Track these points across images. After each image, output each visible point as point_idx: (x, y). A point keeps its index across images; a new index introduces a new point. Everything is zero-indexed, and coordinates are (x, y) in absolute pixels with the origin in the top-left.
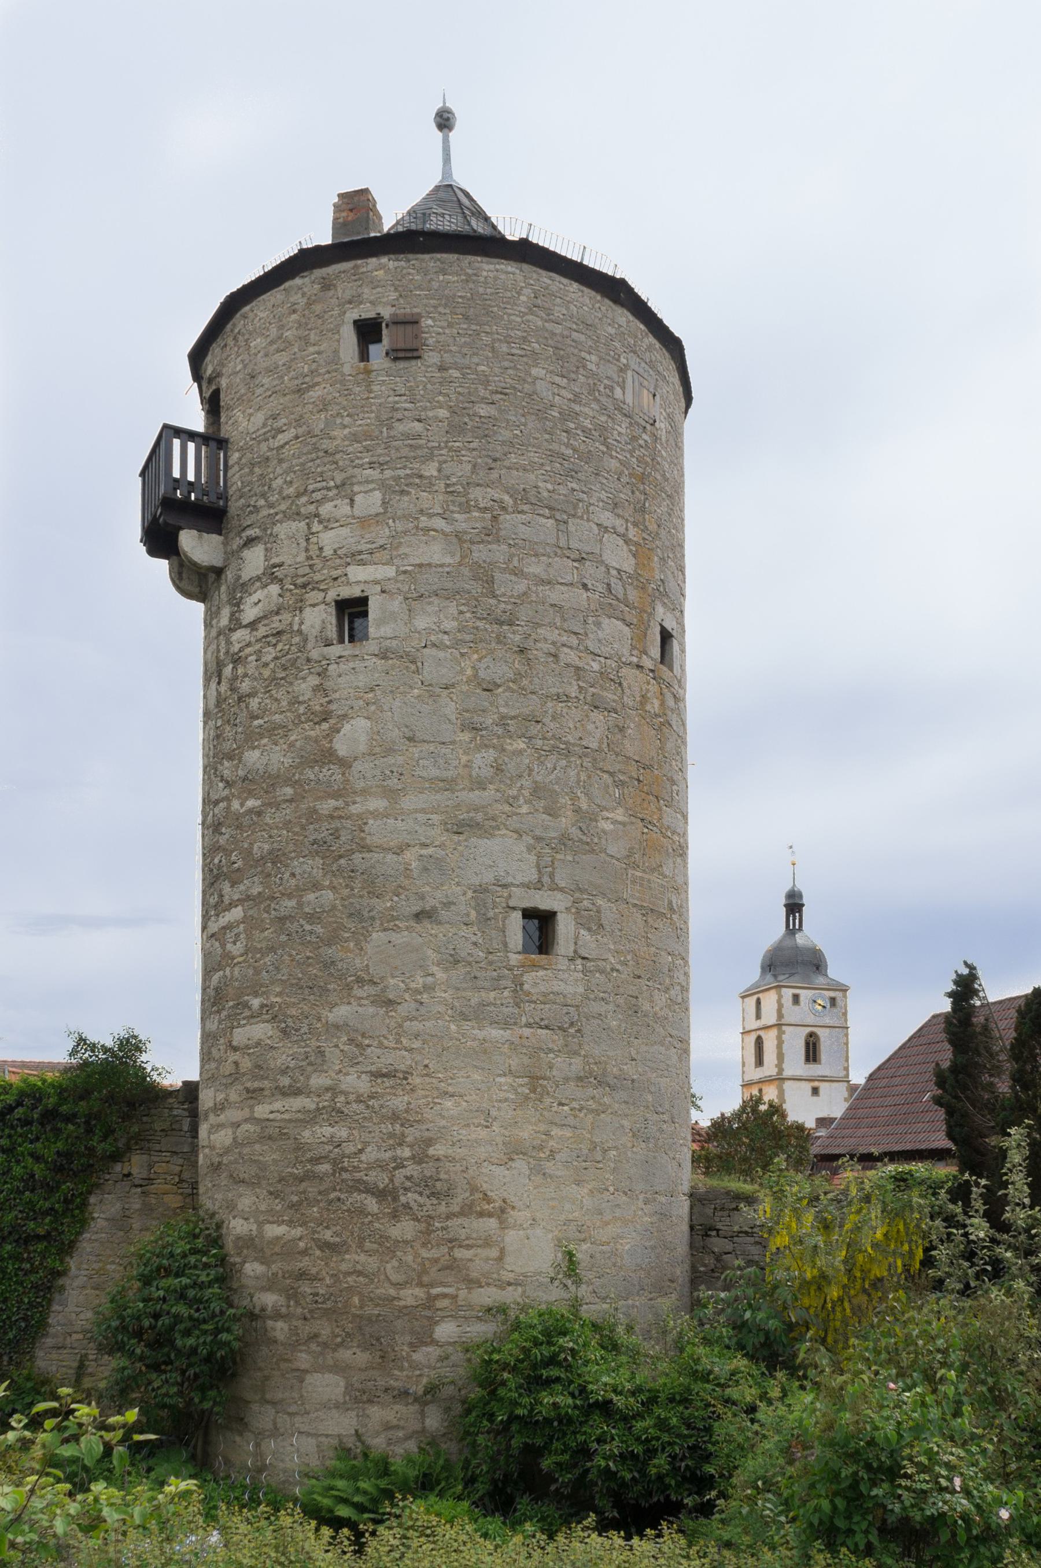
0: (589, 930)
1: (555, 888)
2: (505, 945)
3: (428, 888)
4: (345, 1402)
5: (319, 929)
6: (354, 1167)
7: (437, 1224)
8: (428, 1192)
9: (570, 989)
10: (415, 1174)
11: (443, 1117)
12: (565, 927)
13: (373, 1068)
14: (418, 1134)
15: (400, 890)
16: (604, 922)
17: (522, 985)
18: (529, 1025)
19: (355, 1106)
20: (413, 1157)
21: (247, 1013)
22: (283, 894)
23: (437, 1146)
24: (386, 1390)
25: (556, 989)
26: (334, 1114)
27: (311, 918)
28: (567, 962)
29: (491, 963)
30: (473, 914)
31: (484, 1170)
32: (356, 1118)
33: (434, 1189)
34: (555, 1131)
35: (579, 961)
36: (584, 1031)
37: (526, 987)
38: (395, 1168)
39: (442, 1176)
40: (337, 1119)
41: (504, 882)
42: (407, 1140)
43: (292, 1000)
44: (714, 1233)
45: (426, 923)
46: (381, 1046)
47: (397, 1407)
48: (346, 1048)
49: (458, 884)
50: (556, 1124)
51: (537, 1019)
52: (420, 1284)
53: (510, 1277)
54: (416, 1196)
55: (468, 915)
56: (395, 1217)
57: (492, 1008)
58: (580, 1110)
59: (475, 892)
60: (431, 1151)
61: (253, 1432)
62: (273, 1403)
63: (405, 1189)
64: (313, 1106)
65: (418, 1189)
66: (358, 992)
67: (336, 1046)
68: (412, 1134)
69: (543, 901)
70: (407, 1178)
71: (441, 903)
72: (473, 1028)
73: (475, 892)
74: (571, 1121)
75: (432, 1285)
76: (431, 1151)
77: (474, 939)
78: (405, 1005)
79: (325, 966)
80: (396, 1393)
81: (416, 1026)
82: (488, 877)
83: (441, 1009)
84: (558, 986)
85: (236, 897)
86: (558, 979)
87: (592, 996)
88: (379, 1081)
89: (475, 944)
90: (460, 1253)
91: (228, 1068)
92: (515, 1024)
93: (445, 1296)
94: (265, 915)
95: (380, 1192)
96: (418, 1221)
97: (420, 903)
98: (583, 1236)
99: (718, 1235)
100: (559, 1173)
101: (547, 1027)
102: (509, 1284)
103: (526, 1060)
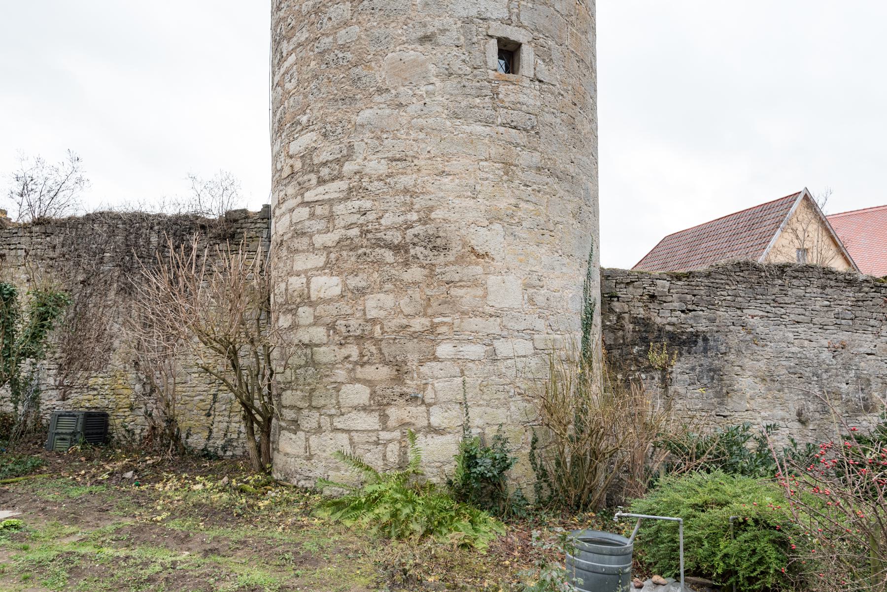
0: (544, 61)
1: (520, 26)
2: (486, 63)
3: (429, 19)
4: (370, 405)
5: (349, 55)
6: (376, 229)
7: (437, 270)
8: (431, 246)
9: (531, 102)
10: (421, 232)
11: (442, 190)
12: (527, 55)
13: (390, 155)
14: (423, 203)
15: (409, 21)
16: (553, 57)
17: (498, 94)
18: (503, 125)
19: (376, 183)
20: (420, 220)
21: (299, 128)
22: (323, 34)
23: (437, 212)
24: (401, 395)
25: (521, 100)
26: (361, 191)
27: (343, 48)
28: (529, 81)
29: (475, 76)
30: (462, 38)
31: (472, 230)
32: (377, 192)
33: (436, 244)
34: (522, 205)
35: (537, 83)
36: (541, 134)
37: (501, 96)
38: (406, 229)
39: (441, 234)
40: (363, 195)
41: (484, 16)
42: (415, 207)
43: (330, 111)
44: (616, 299)
45: (428, 46)
46: (395, 138)
47: (409, 408)
48: (369, 141)
49: (450, 16)
50: (522, 200)
51: (509, 121)
52: (425, 315)
53: (492, 311)
54: (422, 249)
55: (458, 39)
56: (407, 264)
57: (476, 110)
58: (539, 192)
59: (463, 22)
60: (433, 216)
61: (303, 431)
62: (317, 408)
63: (414, 244)
64: (346, 186)
65: (423, 243)
66: (377, 98)
67: (362, 140)
68: (419, 203)
69: (514, 34)
70: (415, 236)
71: (439, 29)
72: (463, 124)
73: (463, 22)
74: (533, 198)
75: (433, 316)
76: (433, 216)
77: (463, 57)
78: (413, 106)
79: (354, 82)
80: (408, 397)
81: (421, 122)
82: (473, 12)
83: (440, 109)
84: (522, 98)
85: (291, 47)
86: (521, 93)
87: (546, 109)
88: (394, 163)
89: (464, 61)
90: (454, 292)
91: (287, 171)
92: (493, 123)
93: (445, 323)
94: (311, 53)
95: (395, 246)
96: (424, 267)
97: (423, 29)
98: (541, 284)
99: (618, 300)
100: (524, 236)
101: (515, 128)
102: (491, 316)
103: (501, 150)
